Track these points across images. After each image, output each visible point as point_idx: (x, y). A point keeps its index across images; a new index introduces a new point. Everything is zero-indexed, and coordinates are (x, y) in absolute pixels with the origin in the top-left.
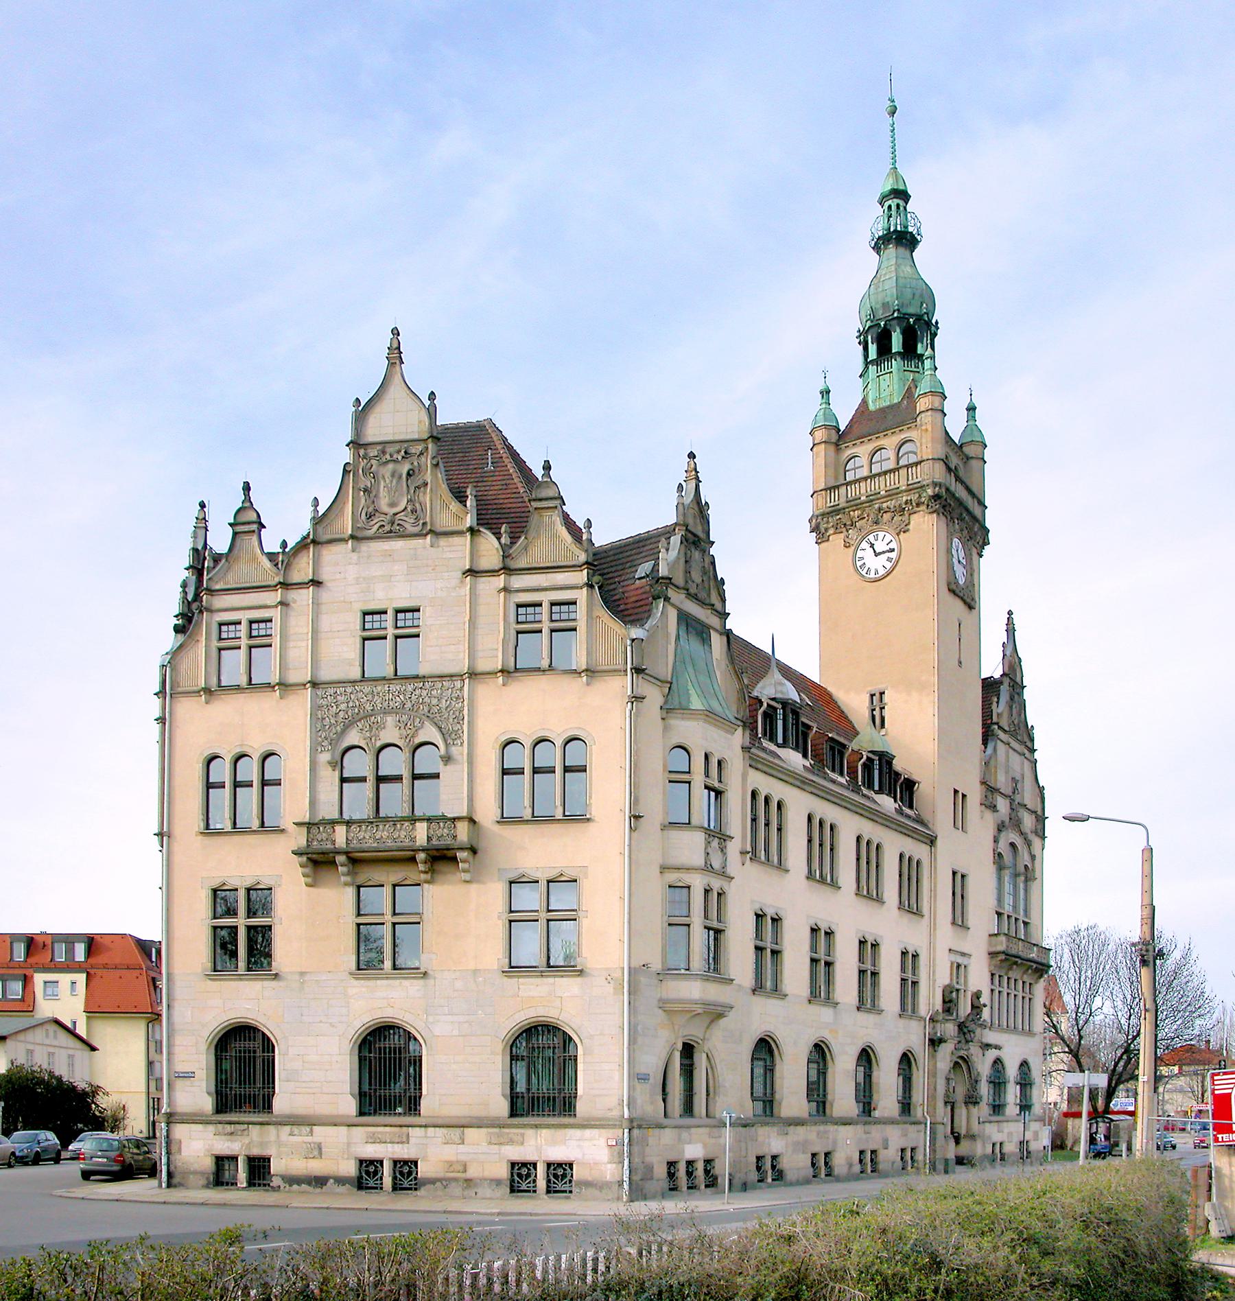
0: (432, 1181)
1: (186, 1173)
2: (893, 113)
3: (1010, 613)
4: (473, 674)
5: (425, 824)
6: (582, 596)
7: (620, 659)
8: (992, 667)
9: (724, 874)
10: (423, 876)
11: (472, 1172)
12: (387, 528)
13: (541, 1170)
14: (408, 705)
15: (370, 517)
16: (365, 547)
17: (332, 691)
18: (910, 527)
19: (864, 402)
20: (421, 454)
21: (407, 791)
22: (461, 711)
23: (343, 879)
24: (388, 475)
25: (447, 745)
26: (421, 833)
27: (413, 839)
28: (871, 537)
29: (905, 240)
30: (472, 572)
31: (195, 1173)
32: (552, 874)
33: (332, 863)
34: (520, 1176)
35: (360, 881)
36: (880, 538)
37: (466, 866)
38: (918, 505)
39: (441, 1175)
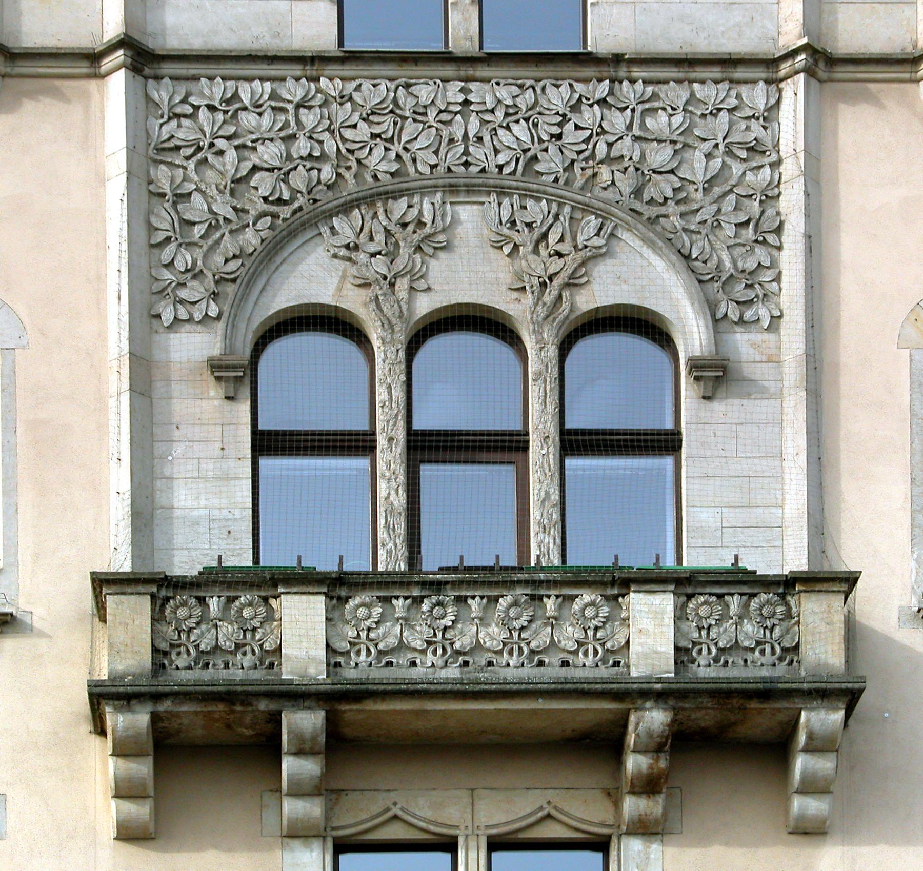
4: (824, 64)
5: (664, 602)
10: (631, 805)
14: (551, 163)
17: (217, 91)
21: (391, 492)
22: (770, 197)
23: (292, 807)
25: (718, 322)
26: (650, 631)
27: (617, 655)
33: (266, 748)
35: (355, 817)
37: (824, 765)
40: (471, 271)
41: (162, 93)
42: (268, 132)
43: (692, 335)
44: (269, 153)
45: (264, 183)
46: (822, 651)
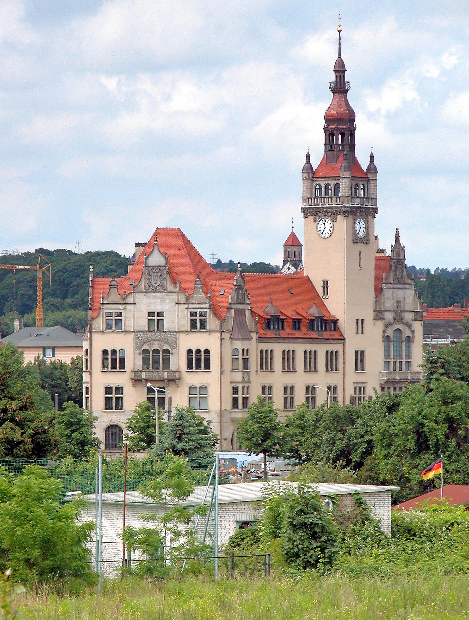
3: (397, 229)
6: (208, 311)
9: (249, 382)
12: (154, 290)
15: (150, 286)
16: (148, 294)
18: (337, 220)
24: (155, 276)
28: (323, 220)
32: (201, 385)
36: (327, 221)
38: (340, 212)
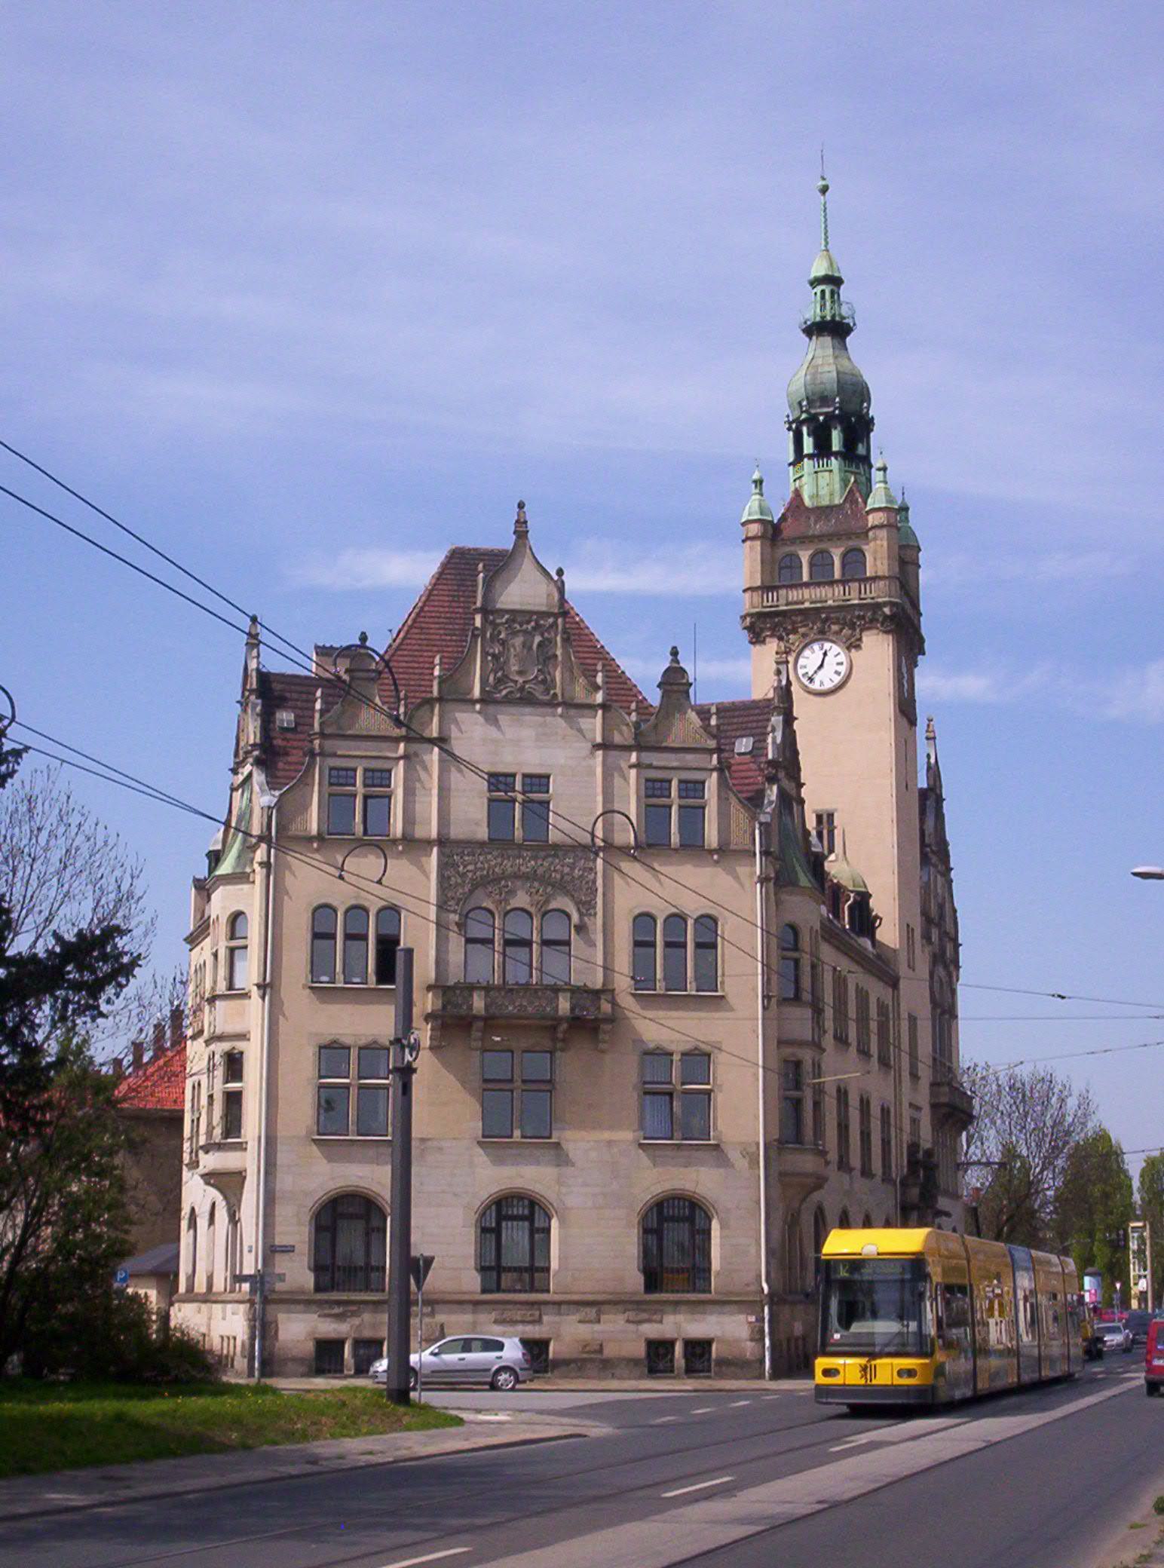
0: (566, 1362)
1: (286, 1361)
2: (824, 190)
4: (609, 846)
7: (747, 840)
8: (923, 783)
11: (609, 1351)
13: (679, 1349)
19: (798, 494)
20: (551, 626)
22: (594, 881)
25: (581, 915)
29: (833, 329)
30: (605, 746)
31: (294, 1360)
34: (657, 1357)
38: (871, 621)
39: (575, 1356)
40: (521, 899)
41: (447, 851)
42: (471, 866)
43: (575, 918)
44: (471, 867)
45: (470, 875)
46: (606, 1007)
